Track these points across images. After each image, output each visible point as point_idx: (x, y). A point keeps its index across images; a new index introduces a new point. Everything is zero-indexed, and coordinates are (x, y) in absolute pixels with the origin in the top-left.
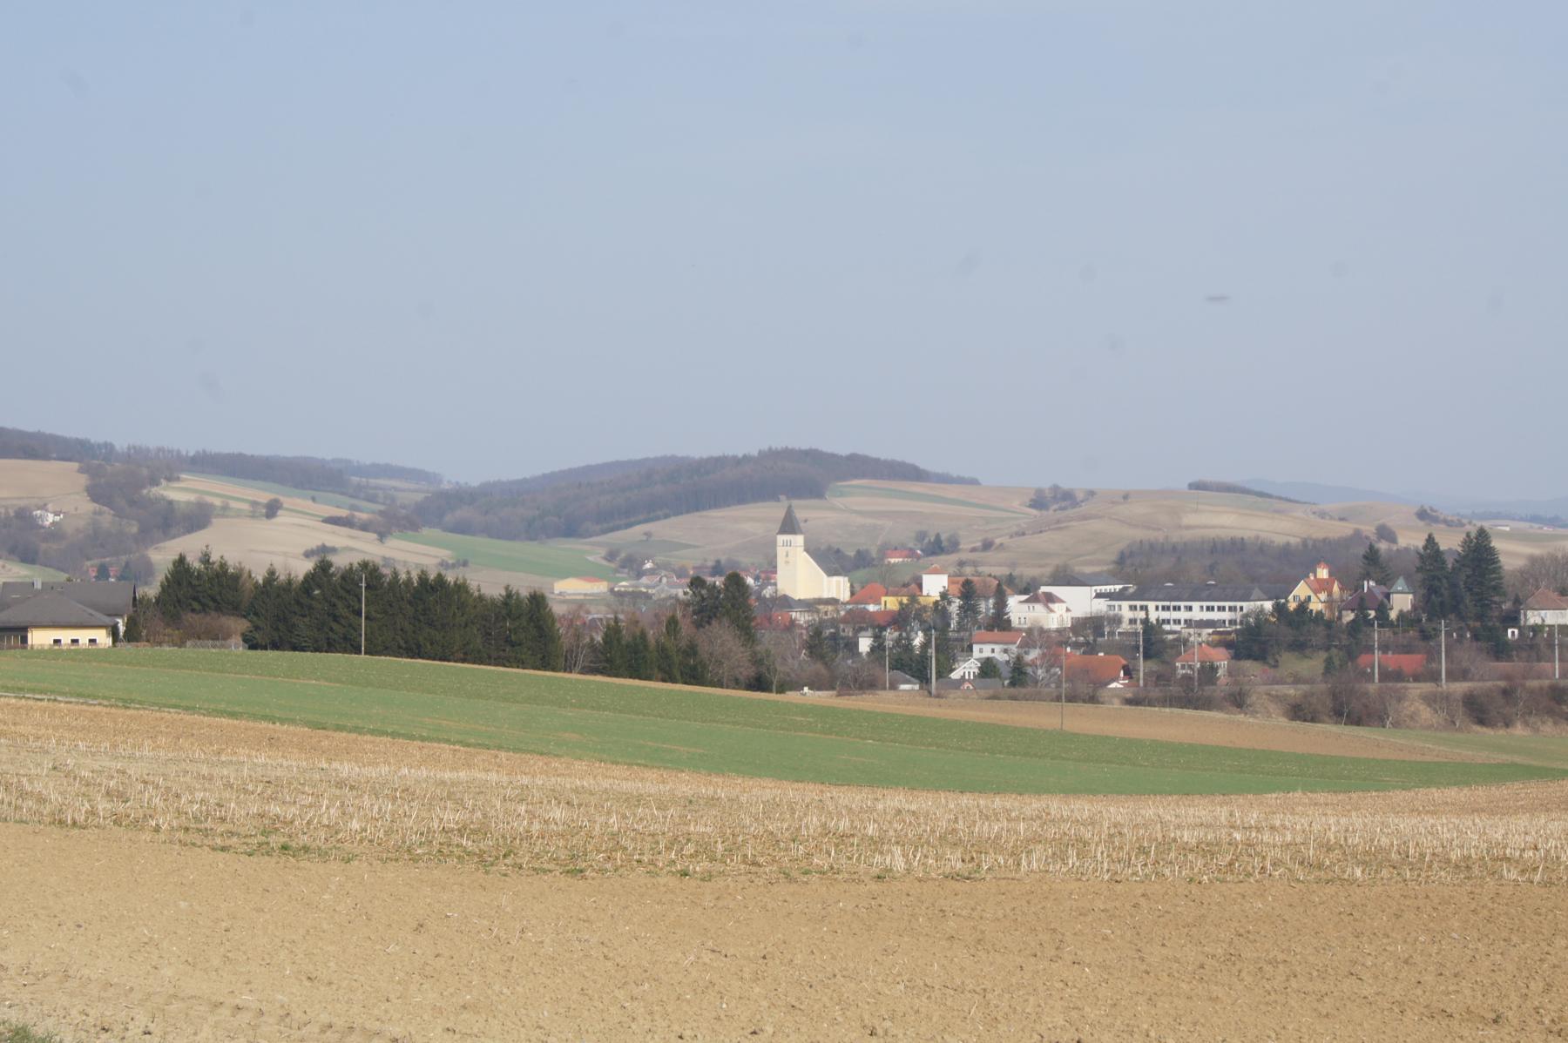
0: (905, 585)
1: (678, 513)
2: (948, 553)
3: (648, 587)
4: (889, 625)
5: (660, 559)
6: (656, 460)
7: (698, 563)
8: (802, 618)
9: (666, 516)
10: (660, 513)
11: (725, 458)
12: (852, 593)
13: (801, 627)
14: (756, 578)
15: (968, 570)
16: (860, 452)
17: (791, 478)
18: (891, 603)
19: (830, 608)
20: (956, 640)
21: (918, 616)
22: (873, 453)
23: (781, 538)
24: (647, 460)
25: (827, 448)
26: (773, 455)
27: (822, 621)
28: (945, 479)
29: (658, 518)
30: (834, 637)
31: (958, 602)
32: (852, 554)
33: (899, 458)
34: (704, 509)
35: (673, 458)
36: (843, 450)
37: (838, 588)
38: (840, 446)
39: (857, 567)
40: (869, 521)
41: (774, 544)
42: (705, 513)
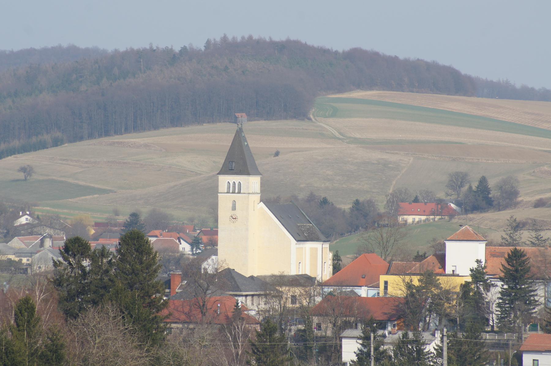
0: (420, 258)
1: (77, 138)
2: (500, 208)
3: (20, 253)
4: (390, 320)
5: (42, 210)
6: (45, 52)
7: (102, 218)
8: (254, 307)
9: (57, 143)
10: (47, 137)
11: (152, 52)
12: (336, 268)
13: (250, 320)
14: (195, 243)
15: (526, 235)
16: (367, 46)
17: (251, 87)
18: (396, 286)
19: (298, 291)
20: (496, 345)
21: (436, 307)
22: (387, 48)
23: (225, 181)
24: (31, 52)
25: (314, 39)
26: (228, 49)
27: (285, 313)
28: (502, 91)
29: (42, 146)
30: (303, 337)
31: (499, 287)
32: (347, 207)
33: (428, 59)
34: (117, 132)
35: (73, 50)
36: (340, 44)
37: (313, 260)
38: (337, 39)
39: (353, 228)
40: (376, 155)
41: (214, 191)
42: (116, 139)
